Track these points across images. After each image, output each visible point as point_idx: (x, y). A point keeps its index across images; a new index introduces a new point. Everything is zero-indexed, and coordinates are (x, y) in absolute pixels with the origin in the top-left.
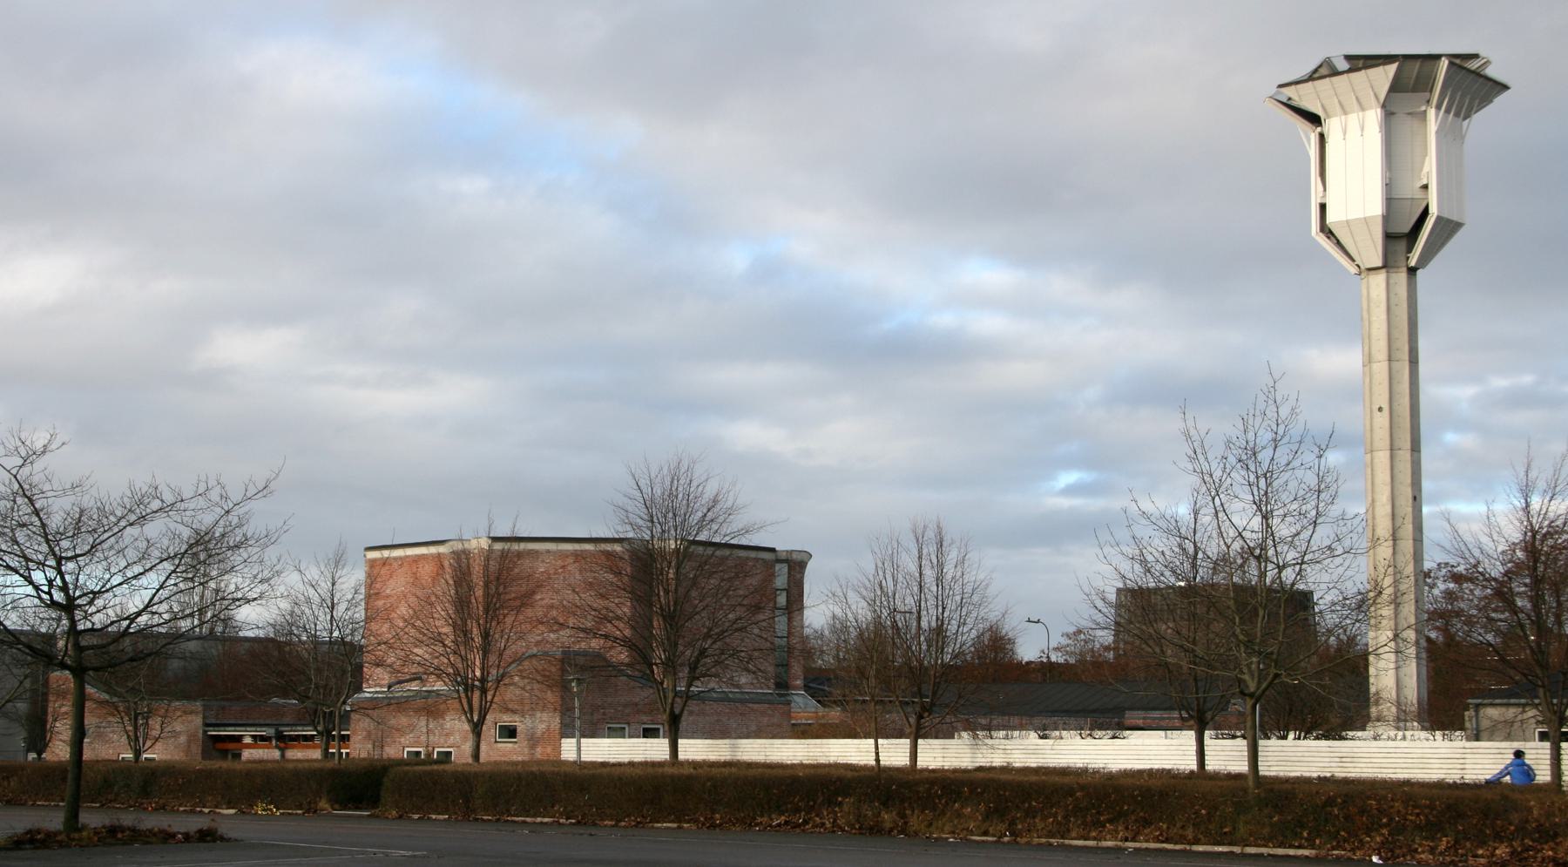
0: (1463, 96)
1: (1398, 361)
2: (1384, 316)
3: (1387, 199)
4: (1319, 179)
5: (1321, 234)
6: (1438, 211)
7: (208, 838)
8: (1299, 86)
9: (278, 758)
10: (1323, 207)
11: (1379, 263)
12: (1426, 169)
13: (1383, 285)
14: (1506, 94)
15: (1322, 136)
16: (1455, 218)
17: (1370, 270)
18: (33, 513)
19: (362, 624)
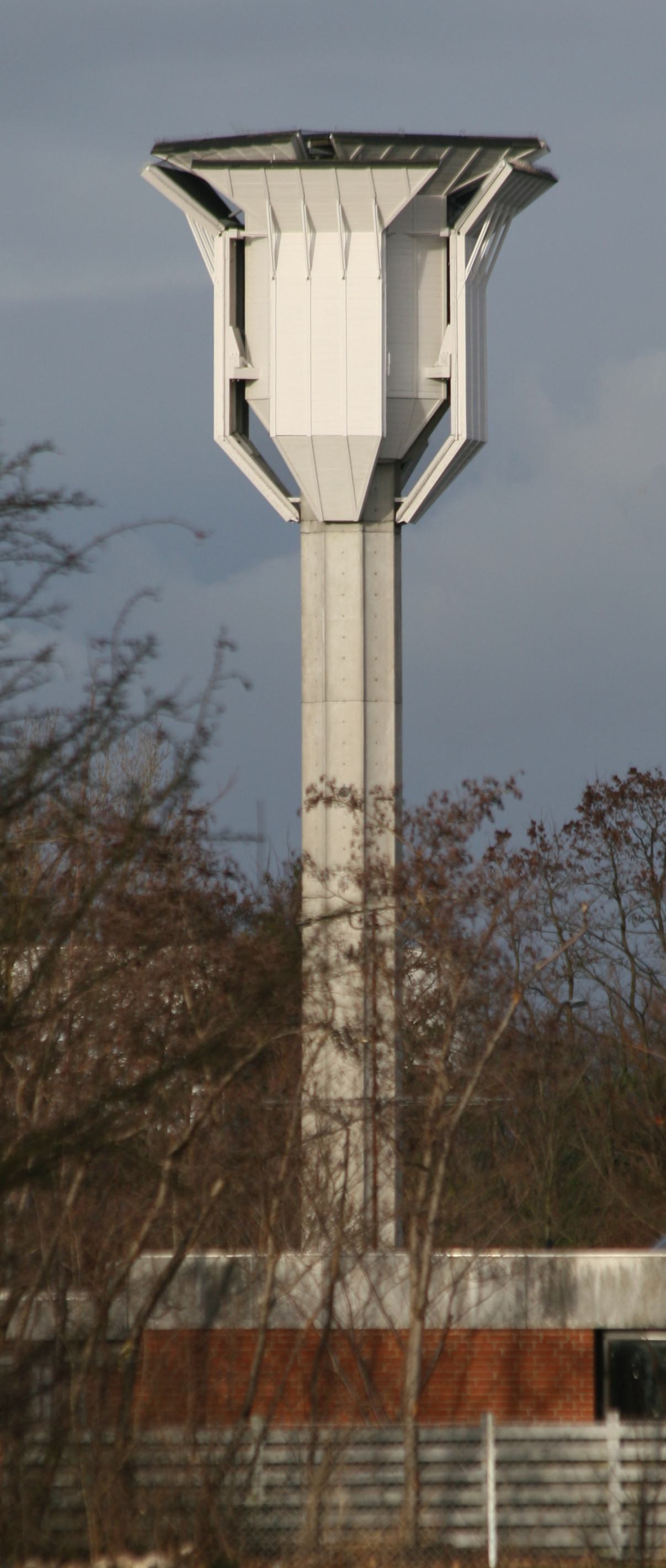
0: (504, 209)
1: (376, 701)
2: (355, 615)
3: (388, 398)
4: (230, 331)
5: (231, 438)
6: (469, 432)
7: (413, 1179)
8: (272, 173)
9: (332, 1113)
10: (239, 387)
11: (356, 518)
12: (446, 349)
13: (356, 555)
14: (553, 191)
15: (239, 247)
16: (479, 439)
17: (328, 523)
18: (565, 976)
19: (455, 1052)
